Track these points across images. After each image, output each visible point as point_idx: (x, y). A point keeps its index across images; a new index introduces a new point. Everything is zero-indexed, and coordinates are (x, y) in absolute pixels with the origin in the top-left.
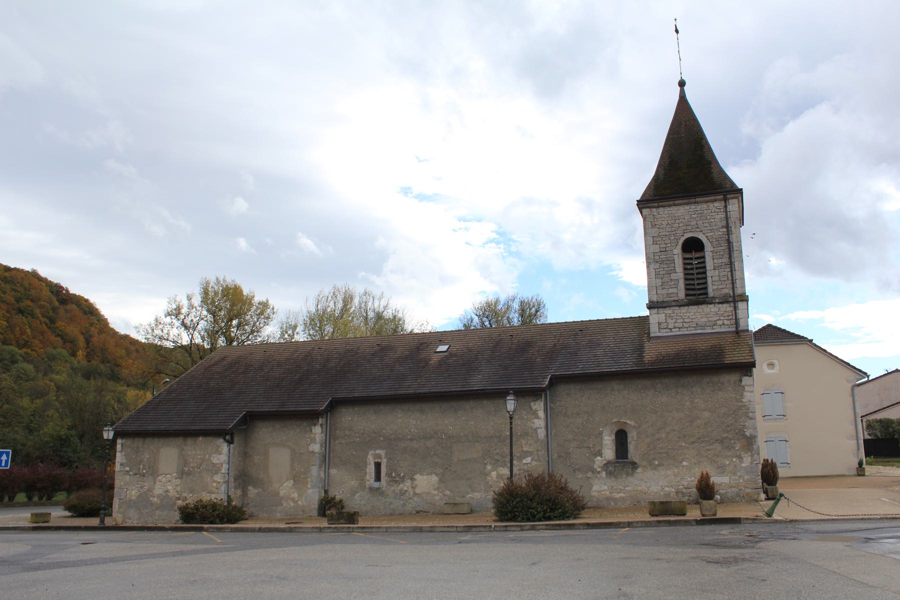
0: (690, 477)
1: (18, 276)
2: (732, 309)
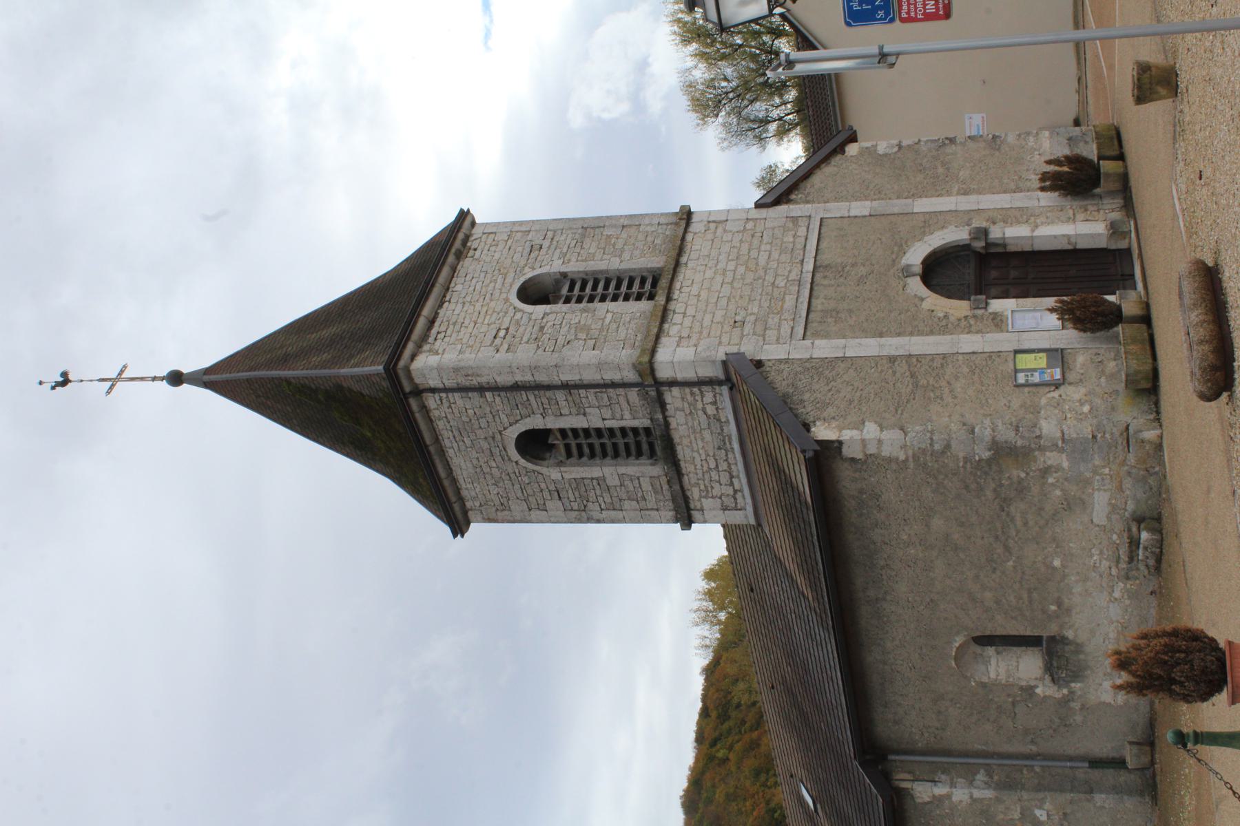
0: (1091, 556)
1: (715, 697)
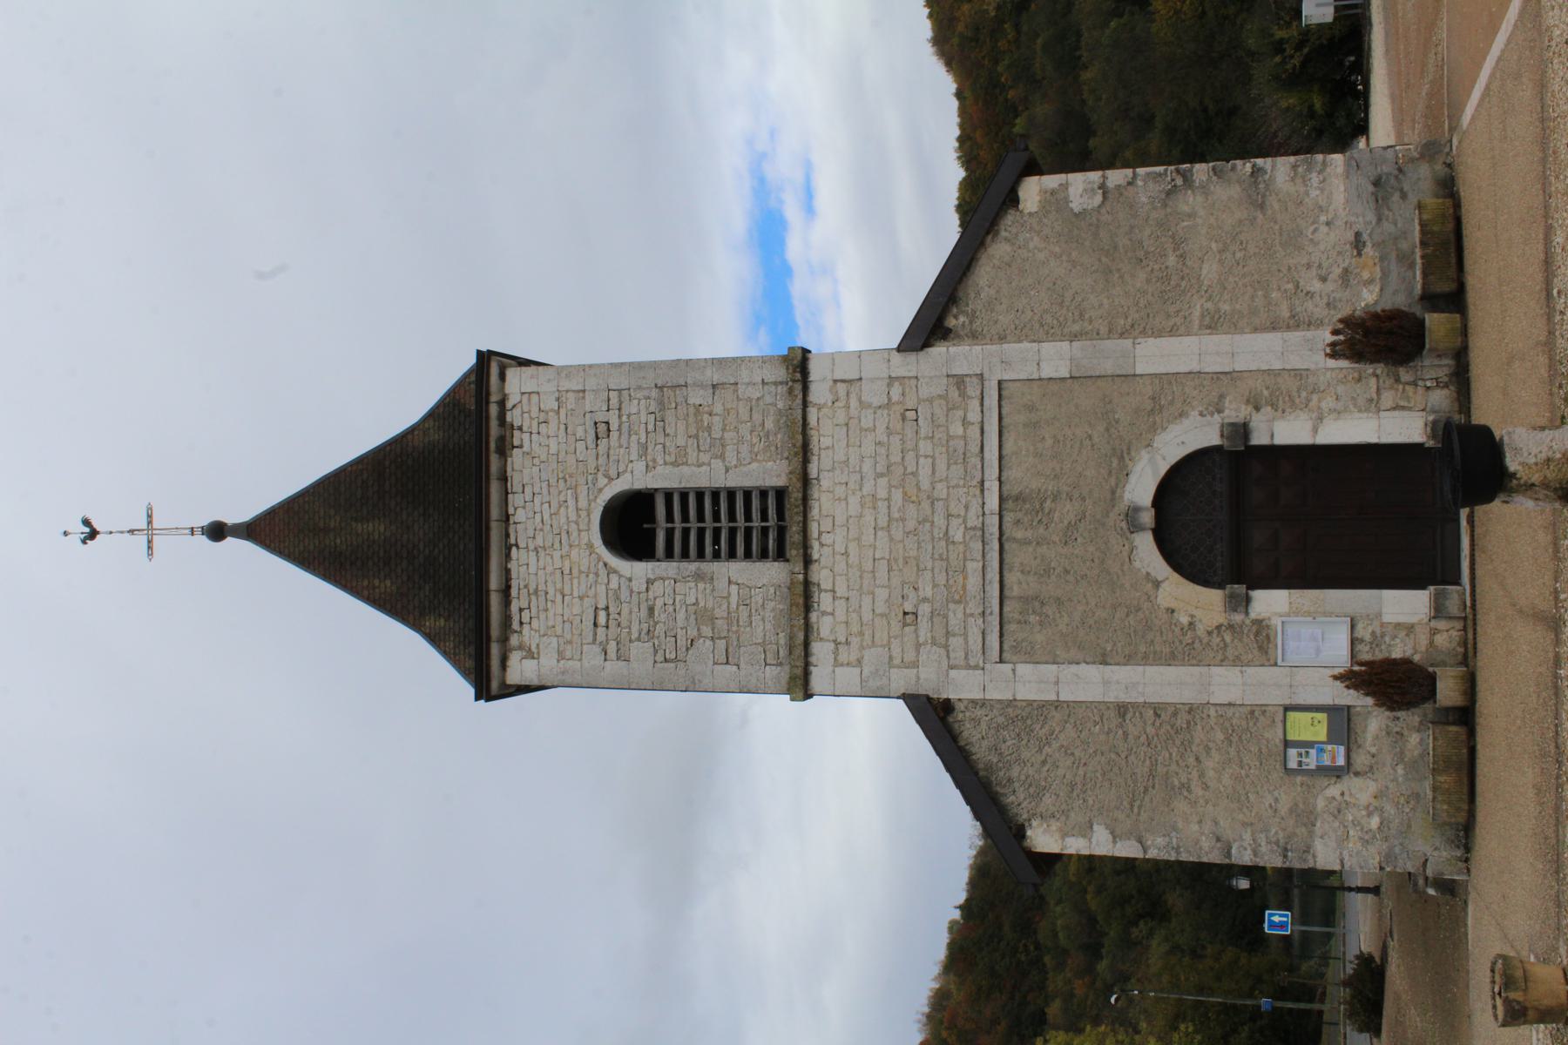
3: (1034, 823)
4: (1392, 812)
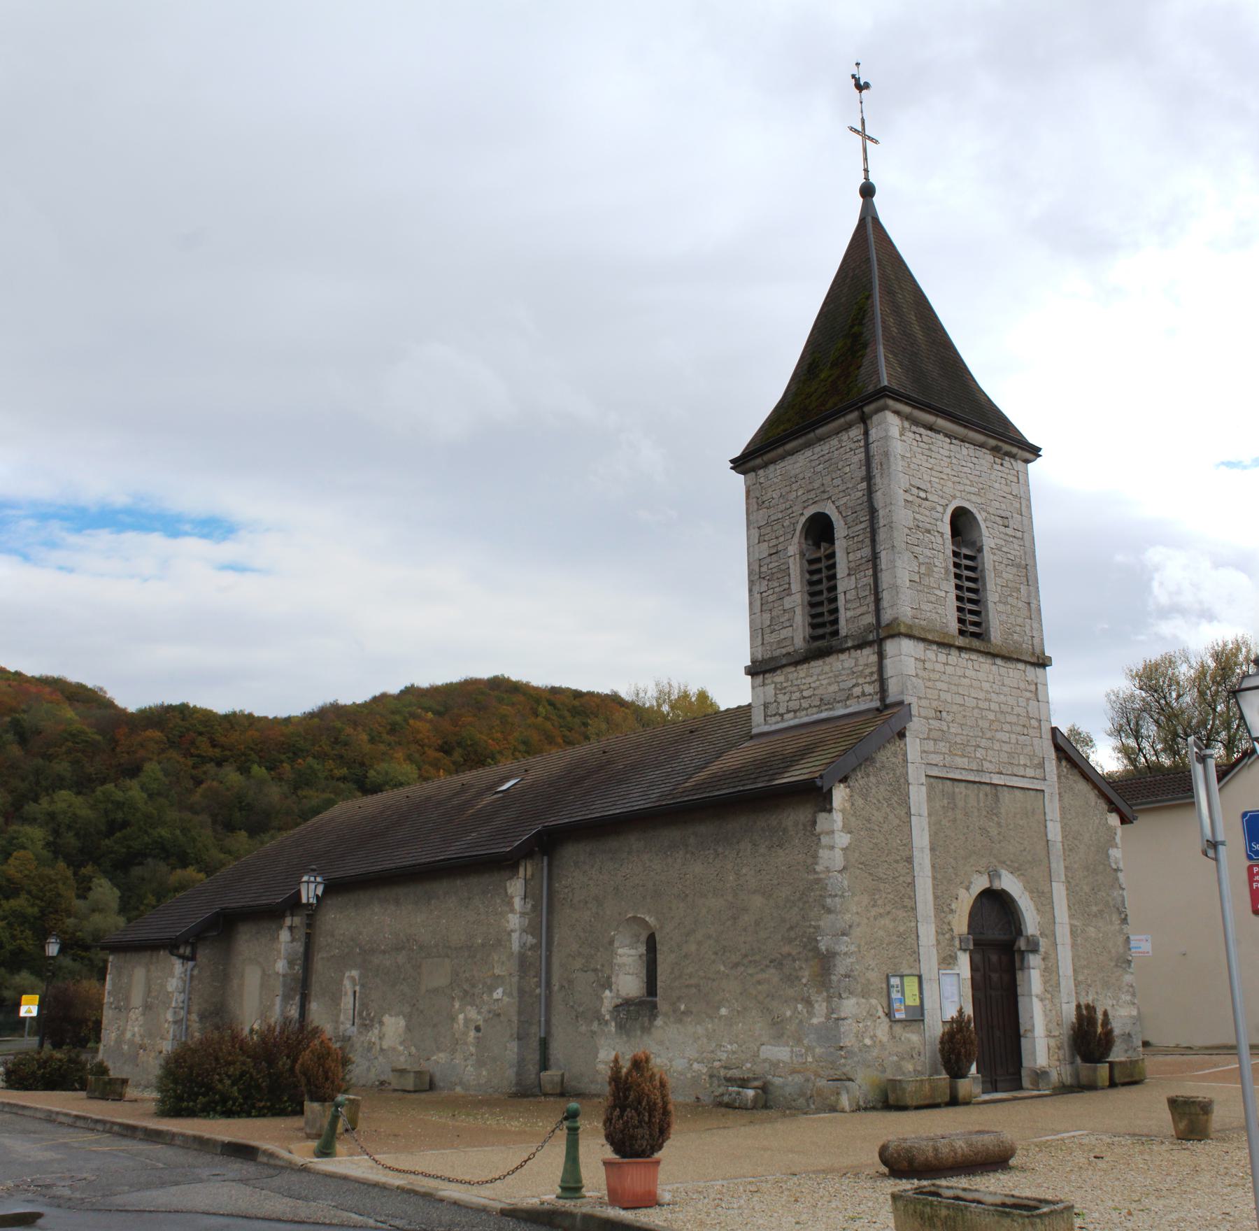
0: (731, 1044)
2: (874, 658)
3: (848, 790)
4: (874, 1054)
